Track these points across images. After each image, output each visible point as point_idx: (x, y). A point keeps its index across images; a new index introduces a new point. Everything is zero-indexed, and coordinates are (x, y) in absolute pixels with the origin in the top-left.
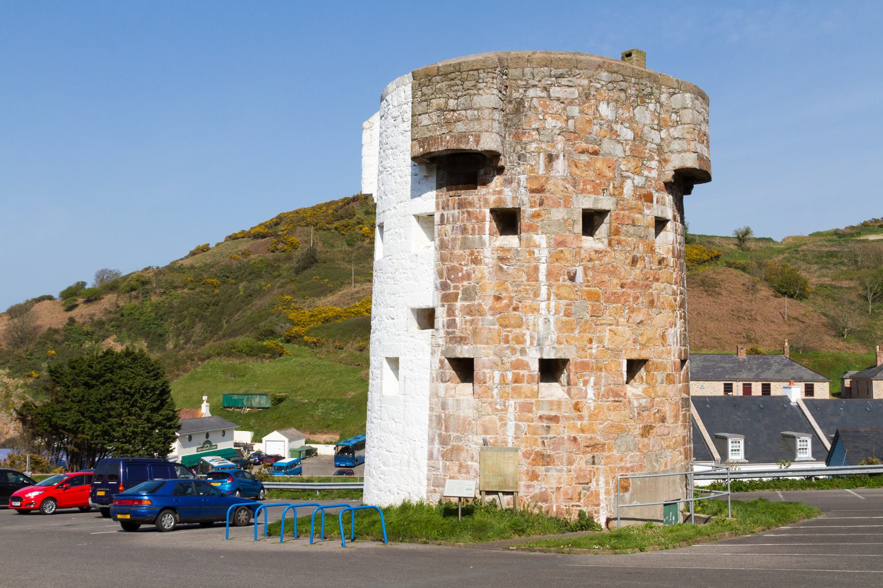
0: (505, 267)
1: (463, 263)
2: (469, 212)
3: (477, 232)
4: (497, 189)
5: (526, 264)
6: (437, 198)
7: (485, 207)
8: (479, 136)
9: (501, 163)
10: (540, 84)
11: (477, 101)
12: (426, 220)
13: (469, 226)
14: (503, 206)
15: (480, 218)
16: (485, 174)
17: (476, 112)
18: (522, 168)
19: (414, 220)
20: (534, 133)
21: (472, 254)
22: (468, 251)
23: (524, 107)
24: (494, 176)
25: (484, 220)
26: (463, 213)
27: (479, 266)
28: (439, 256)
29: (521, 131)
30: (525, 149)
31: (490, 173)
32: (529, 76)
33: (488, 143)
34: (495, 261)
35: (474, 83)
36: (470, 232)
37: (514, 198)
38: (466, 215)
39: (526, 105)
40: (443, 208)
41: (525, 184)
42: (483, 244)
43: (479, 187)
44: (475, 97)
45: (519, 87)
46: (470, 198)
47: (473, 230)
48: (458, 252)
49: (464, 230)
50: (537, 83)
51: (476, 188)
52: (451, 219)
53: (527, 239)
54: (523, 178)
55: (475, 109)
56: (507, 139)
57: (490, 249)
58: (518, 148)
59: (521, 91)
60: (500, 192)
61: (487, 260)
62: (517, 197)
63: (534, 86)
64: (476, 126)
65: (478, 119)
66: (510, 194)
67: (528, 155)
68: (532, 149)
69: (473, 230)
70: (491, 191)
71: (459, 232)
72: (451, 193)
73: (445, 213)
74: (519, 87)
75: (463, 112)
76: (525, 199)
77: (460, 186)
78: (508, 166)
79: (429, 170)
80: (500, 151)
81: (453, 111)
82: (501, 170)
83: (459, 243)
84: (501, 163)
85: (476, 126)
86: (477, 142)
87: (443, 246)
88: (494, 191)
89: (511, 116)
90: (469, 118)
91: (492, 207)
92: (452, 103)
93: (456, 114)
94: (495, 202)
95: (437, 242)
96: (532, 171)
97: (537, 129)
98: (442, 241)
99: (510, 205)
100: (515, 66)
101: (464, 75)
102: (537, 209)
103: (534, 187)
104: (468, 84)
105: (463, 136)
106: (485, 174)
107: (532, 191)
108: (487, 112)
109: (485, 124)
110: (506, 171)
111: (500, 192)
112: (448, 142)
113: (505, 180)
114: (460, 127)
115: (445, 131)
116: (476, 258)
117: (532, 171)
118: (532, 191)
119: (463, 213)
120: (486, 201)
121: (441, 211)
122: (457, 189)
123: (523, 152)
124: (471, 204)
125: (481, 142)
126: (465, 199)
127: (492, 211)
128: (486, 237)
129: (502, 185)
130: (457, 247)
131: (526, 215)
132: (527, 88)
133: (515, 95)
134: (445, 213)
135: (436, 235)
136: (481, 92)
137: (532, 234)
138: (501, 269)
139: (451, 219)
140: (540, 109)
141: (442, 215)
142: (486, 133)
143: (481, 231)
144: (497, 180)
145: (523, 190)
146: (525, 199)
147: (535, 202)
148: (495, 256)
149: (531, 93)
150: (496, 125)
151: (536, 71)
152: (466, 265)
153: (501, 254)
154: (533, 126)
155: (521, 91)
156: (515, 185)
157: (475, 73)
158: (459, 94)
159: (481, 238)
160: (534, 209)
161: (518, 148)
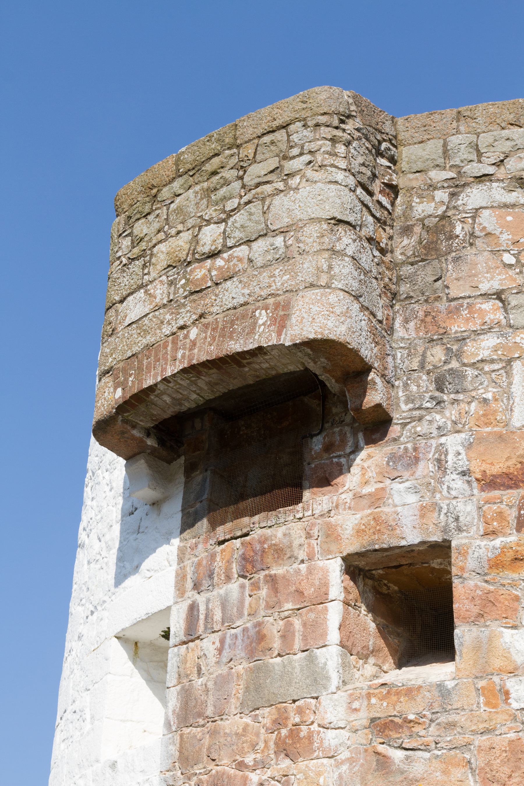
0: (398, 755)
1: (249, 760)
2: (272, 580)
3: (298, 644)
4: (367, 490)
5: (479, 740)
6: (181, 560)
7: (327, 553)
8: (287, 306)
9: (374, 397)
10: (501, 173)
11: (285, 208)
12: (146, 649)
13: (274, 627)
14: (387, 541)
15: (309, 591)
16: (328, 448)
17: (279, 241)
18: (451, 413)
19: (119, 654)
20: (487, 306)
21: (279, 722)
22: (267, 715)
23: (452, 237)
24: (357, 449)
25: (322, 599)
26: (256, 586)
27: (302, 764)
28: (174, 749)
29: (442, 306)
30: (459, 355)
31: (343, 441)
32: (465, 153)
33: (322, 315)
34: (362, 737)
35: (273, 163)
36: (277, 645)
37: (424, 511)
38: (264, 592)
39: (458, 230)
40: (197, 587)
41: (463, 463)
42: (317, 678)
43: (307, 495)
44: (277, 201)
45: (432, 187)
46: (279, 532)
47: (286, 636)
48: (234, 722)
49: (257, 642)
50: (491, 170)
51: (298, 499)
52: (218, 615)
53: (477, 647)
54: (453, 443)
55: (276, 232)
56: (400, 332)
57: (342, 696)
58: (437, 354)
59: (441, 195)
60: (377, 499)
61: (331, 738)
62: (436, 507)
63: (482, 178)
64: (281, 279)
65: (286, 258)
66: (412, 499)
67: (470, 372)
68: (484, 354)
69: (286, 636)
70: (347, 497)
71: (240, 653)
72: (221, 532)
73: (201, 599)
74: (432, 187)
75: (242, 251)
76: (467, 510)
77: (250, 502)
78: (400, 412)
79: (161, 477)
80: (368, 352)
81: (213, 255)
82: (377, 425)
83: (237, 690)
84: (374, 397)
85: (281, 279)
86: (281, 323)
87: (188, 713)
88: (358, 497)
89: (407, 270)
90: (259, 261)
91: (352, 547)
92: (210, 237)
93: (219, 262)
94: (359, 532)
95: (173, 697)
96: (487, 418)
97: (499, 295)
98: (186, 695)
99: (411, 536)
100: (419, 137)
101: (248, 151)
102: (513, 538)
103: (496, 469)
104: (256, 171)
105: (242, 312)
106: (328, 448)
107: (490, 483)
108: (312, 231)
109: (307, 268)
110: (394, 430)
111: (377, 499)
112: (194, 343)
113: (393, 458)
114: (233, 293)
115: (186, 317)
116: (294, 734)
117: (487, 418)
118: (490, 483)
119: (256, 586)
120: (331, 534)
121: (191, 595)
122: (238, 515)
123: (454, 364)
124: (280, 552)
125: (294, 320)
126: (263, 541)
127: (356, 568)
128: (330, 656)
129: (382, 475)
130: (233, 706)
131: (471, 564)
132: (457, 187)
133: (423, 208)
134: (201, 599)
135: (171, 679)
136: (294, 182)
137: (495, 627)
138: (383, 763)
139: (218, 615)
140: (505, 237)
141: (193, 608)
142: (311, 294)
143: (315, 633)
144: (368, 462)
145: (458, 484)
146: (467, 510)
147: (501, 515)
148: (362, 718)
149: (474, 197)
150: (344, 269)
151: (484, 140)
152: (261, 765)
153: (382, 709)
154: (485, 287)
155: (441, 195)
156: (426, 468)
157: (281, 135)
158: (230, 205)
159: (312, 660)
160: (498, 542)
161: (437, 354)
